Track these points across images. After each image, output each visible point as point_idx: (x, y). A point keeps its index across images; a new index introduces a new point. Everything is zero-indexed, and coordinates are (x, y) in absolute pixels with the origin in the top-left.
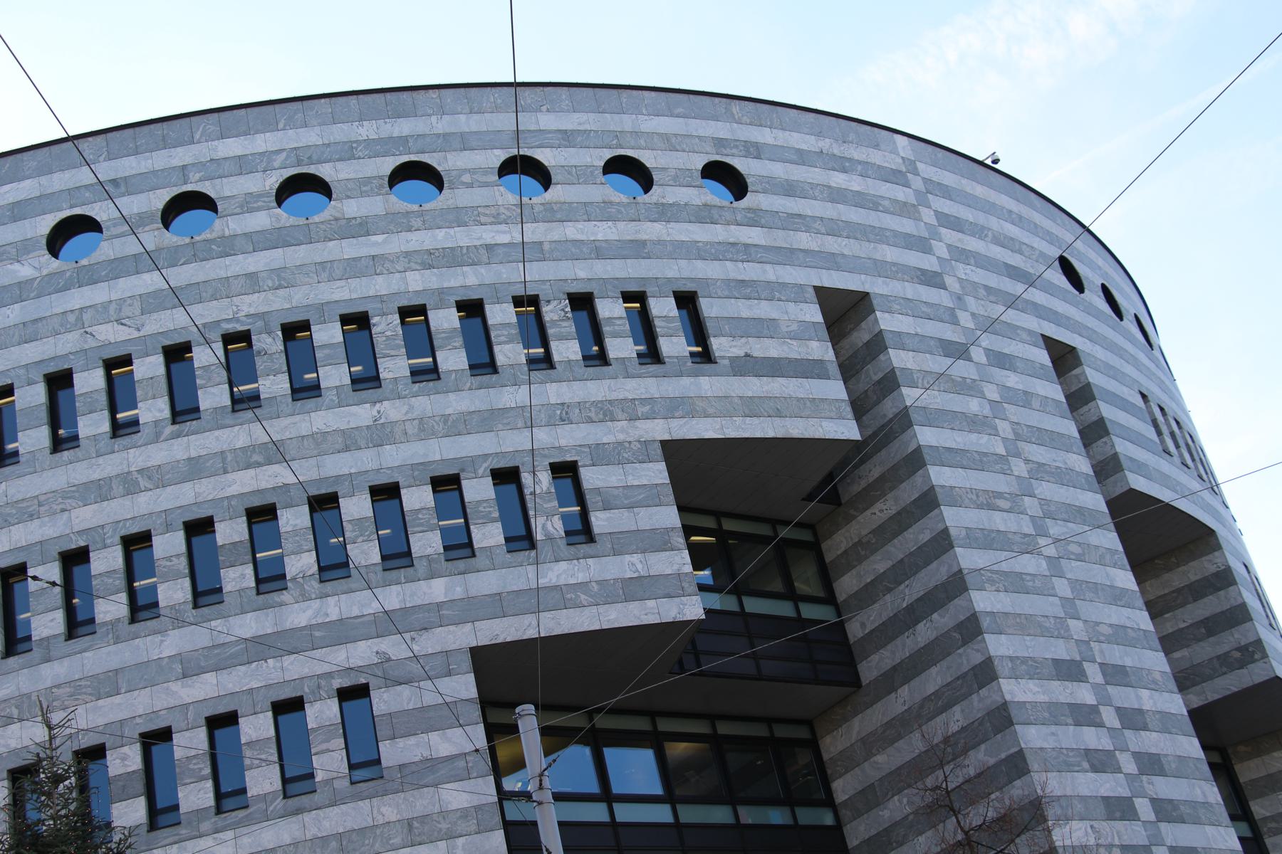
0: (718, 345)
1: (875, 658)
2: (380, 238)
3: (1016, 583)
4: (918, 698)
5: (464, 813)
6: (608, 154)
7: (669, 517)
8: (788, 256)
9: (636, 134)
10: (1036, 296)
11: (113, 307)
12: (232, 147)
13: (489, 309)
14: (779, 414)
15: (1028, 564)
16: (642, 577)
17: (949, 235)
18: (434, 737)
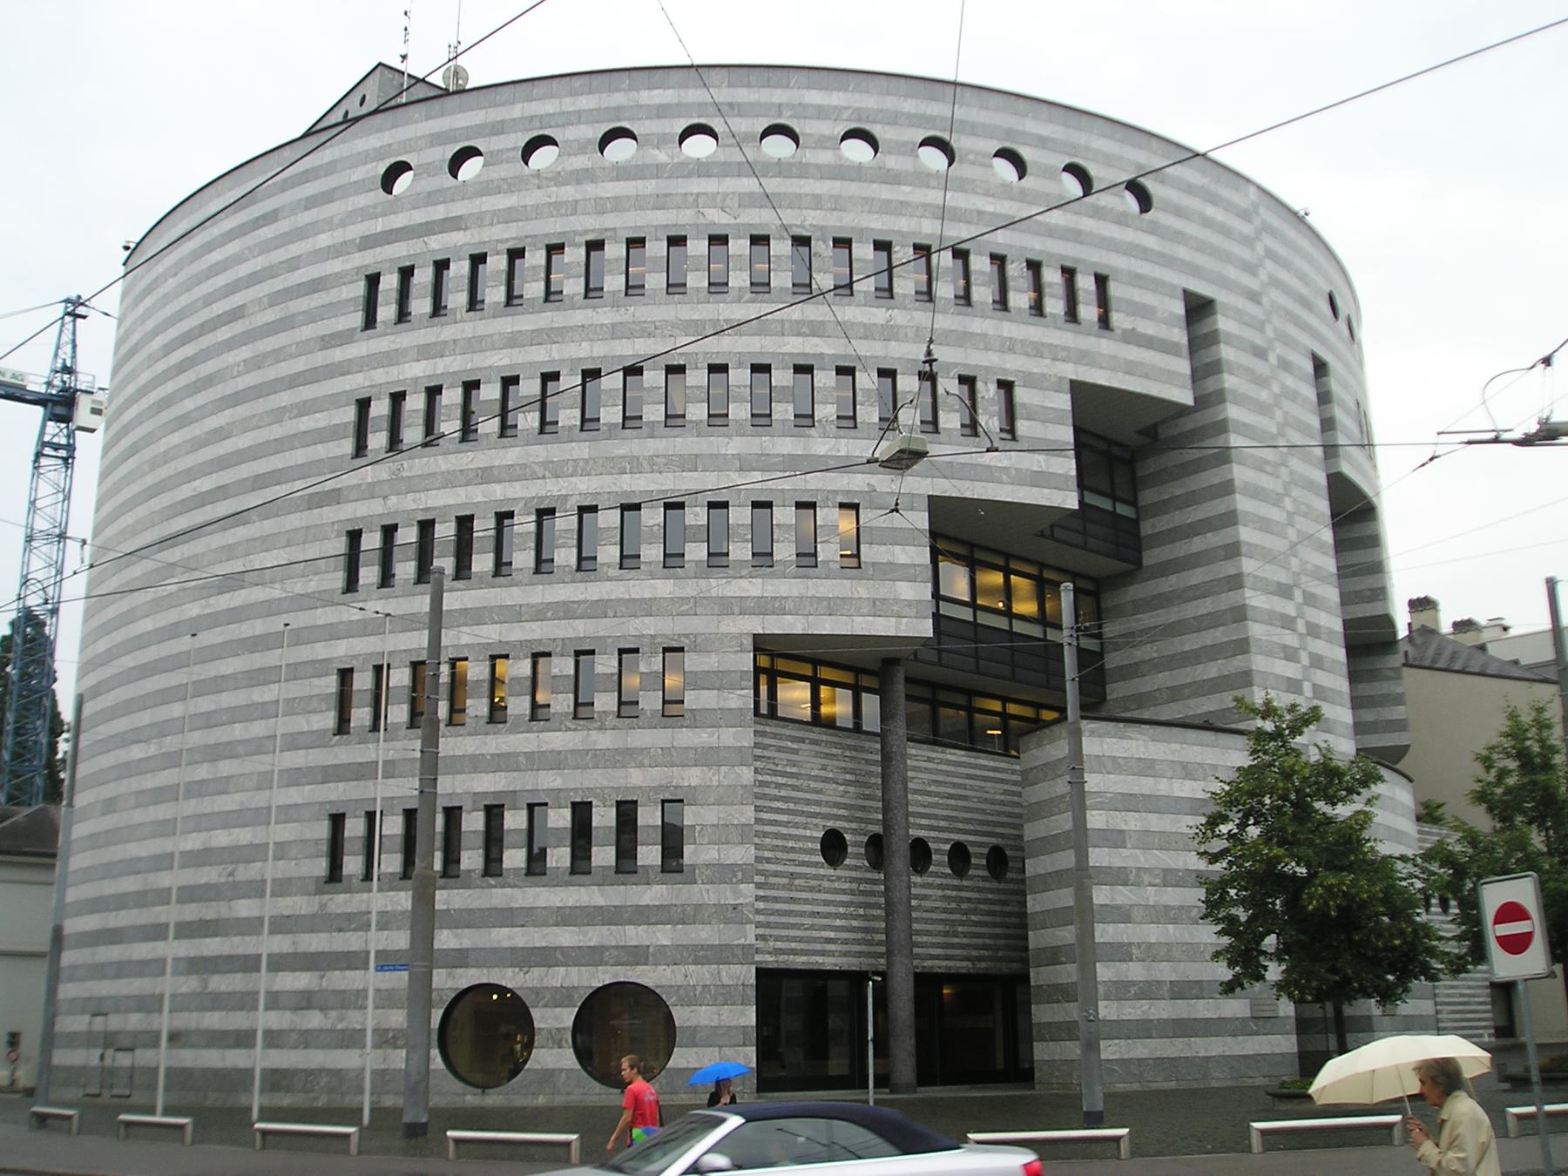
0: (1116, 318)
2: (908, 189)
3: (1266, 526)
4: (1182, 585)
5: (909, 603)
6: (1067, 161)
7: (1066, 435)
8: (1168, 261)
9: (1088, 149)
10: (1304, 315)
11: (719, 198)
12: (814, 97)
13: (972, 258)
14: (1146, 376)
15: (1276, 514)
16: (1039, 474)
17: (1270, 266)
18: (897, 549)
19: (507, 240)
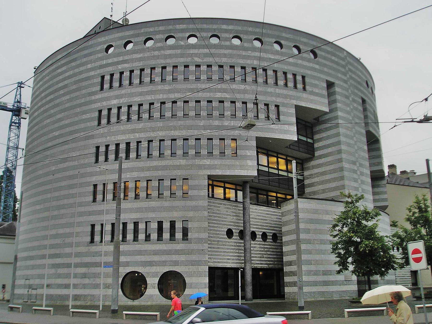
1: (319, 152)
2: (250, 52)
8: (322, 72)
12: (224, 27)
17: (350, 73)
19: (163, 64)
